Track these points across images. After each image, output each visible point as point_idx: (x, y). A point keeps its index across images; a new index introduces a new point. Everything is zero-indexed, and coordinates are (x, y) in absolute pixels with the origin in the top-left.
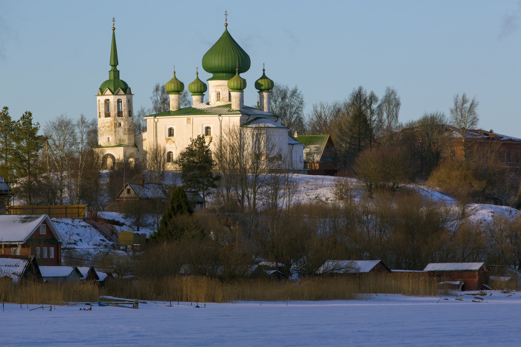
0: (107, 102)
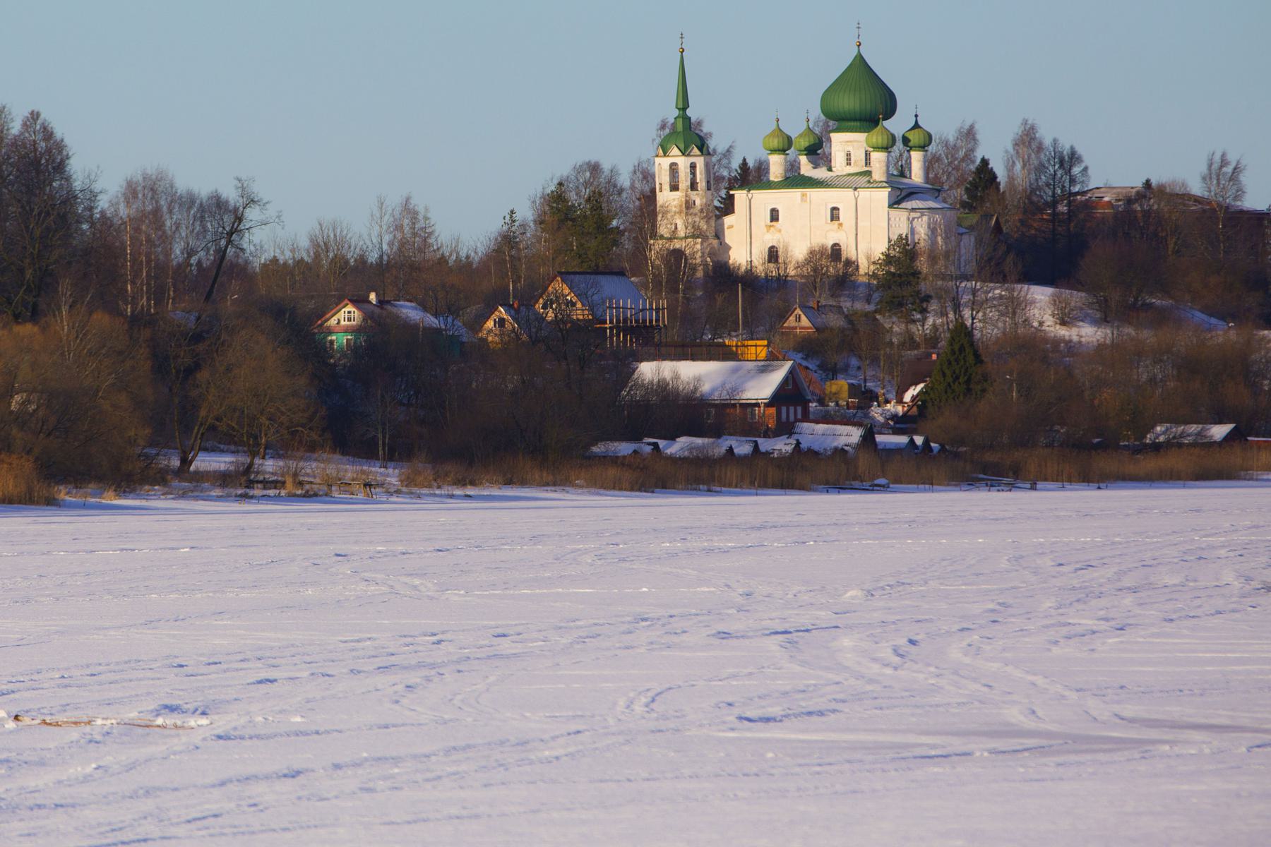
0: (673, 168)
